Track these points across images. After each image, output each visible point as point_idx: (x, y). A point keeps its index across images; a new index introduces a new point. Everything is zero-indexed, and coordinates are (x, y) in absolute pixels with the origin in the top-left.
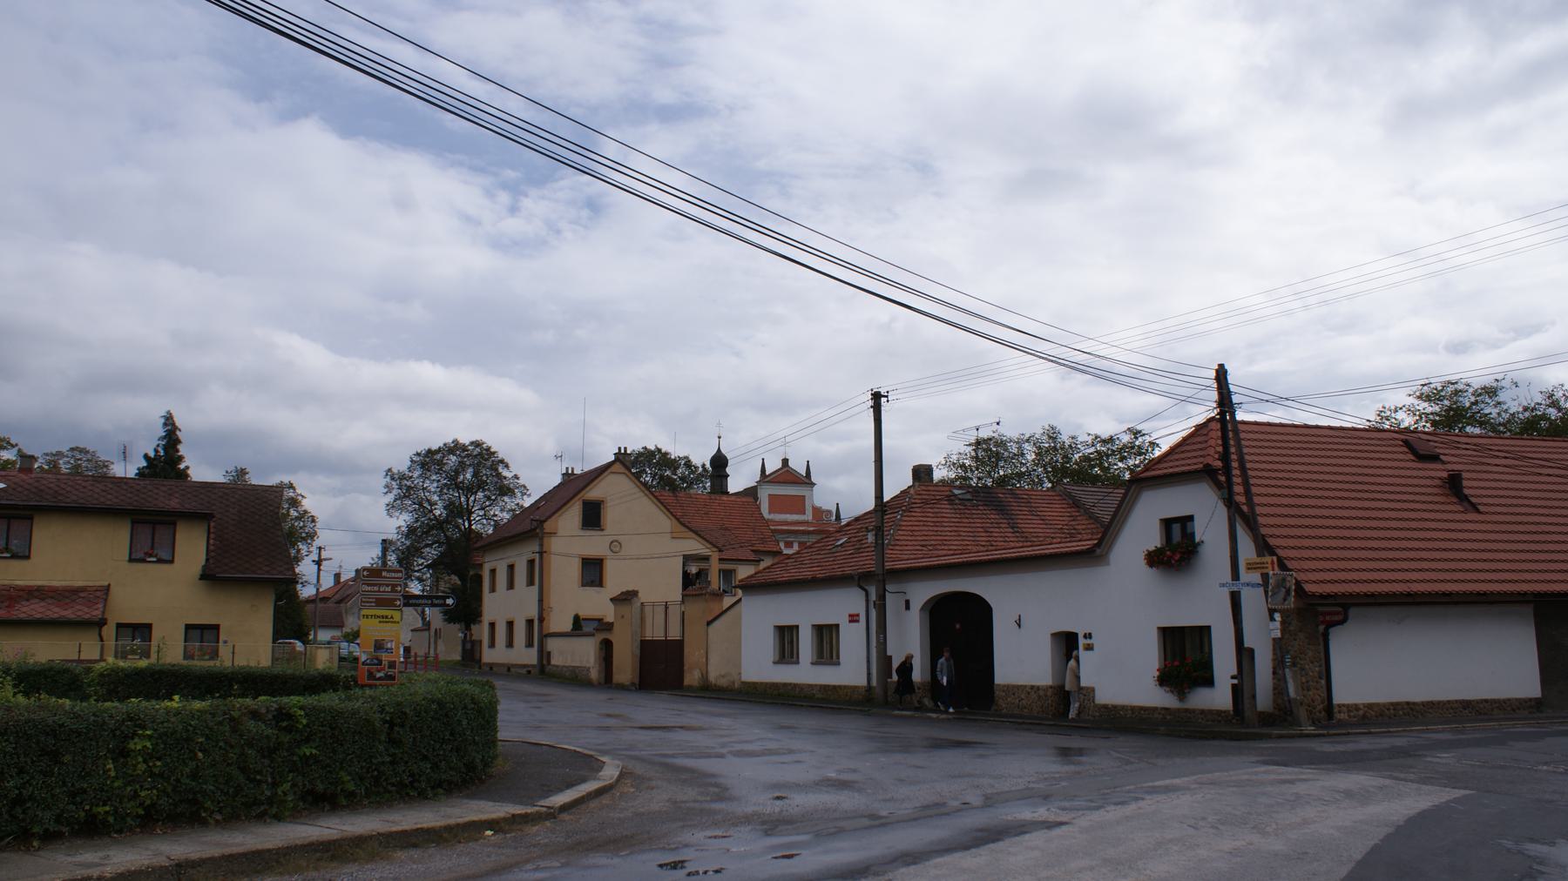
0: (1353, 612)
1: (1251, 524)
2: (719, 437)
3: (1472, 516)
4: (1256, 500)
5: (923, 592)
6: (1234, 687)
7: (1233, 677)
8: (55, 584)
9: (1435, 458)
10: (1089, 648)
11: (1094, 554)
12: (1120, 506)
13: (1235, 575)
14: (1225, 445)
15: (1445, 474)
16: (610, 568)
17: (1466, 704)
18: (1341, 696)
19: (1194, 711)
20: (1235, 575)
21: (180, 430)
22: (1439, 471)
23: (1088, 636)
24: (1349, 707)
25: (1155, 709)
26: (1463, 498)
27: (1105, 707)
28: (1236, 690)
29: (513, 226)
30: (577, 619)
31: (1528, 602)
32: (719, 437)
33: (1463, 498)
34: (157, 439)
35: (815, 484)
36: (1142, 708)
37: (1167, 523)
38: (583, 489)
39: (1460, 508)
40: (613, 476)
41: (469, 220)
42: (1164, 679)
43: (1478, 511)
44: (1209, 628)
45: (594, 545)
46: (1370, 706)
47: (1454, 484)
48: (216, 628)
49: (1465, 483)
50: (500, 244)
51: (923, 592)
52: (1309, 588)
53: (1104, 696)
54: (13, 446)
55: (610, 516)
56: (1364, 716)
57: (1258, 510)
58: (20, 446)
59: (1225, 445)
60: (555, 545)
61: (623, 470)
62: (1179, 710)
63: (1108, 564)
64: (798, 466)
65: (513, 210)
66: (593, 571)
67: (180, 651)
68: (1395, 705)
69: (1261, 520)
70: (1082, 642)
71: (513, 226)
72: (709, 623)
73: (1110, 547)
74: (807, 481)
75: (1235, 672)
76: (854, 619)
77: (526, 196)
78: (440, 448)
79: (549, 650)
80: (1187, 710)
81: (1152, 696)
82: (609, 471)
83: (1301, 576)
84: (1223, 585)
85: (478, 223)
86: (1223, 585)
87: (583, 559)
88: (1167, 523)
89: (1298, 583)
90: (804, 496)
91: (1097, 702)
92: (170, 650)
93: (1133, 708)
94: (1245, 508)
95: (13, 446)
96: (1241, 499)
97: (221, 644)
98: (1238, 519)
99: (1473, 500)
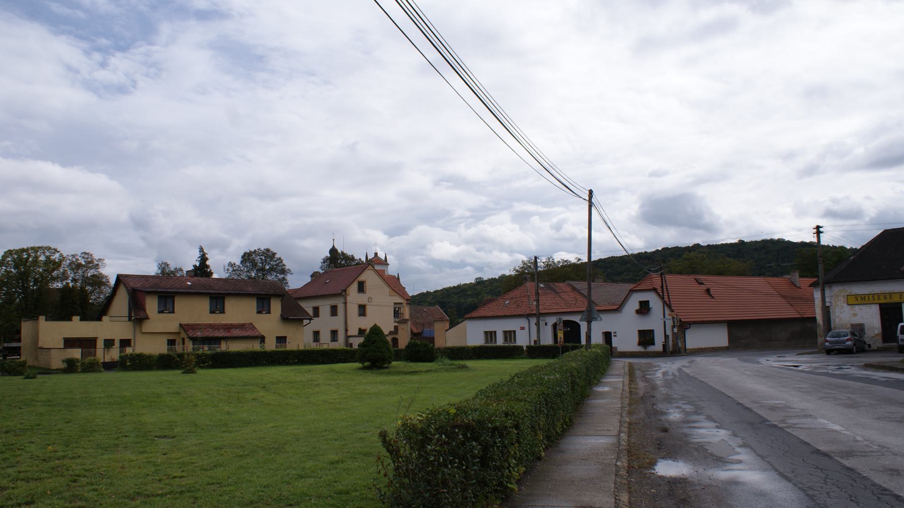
0: (691, 325)
1: (669, 307)
2: (334, 240)
3: (713, 300)
4: (671, 300)
5: (552, 320)
6: (663, 345)
7: (663, 342)
8: (234, 322)
9: (702, 284)
10: (615, 336)
11: (618, 309)
12: (626, 296)
13: (664, 317)
14: (662, 284)
15: (705, 288)
16: (369, 310)
17: (713, 348)
18: (687, 347)
19: (649, 352)
20: (664, 317)
21: (207, 254)
22: (703, 287)
23: (615, 333)
24: (690, 349)
25: (636, 352)
26: (710, 295)
27: (621, 352)
28: (664, 346)
29: (103, 75)
30: (360, 330)
31: (725, 322)
32: (334, 240)
33: (710, 295)
34: (198, 257)
35: (333, 251)
36: (632, 352)
37: (641, 303)
38: (358, 276)
39: (709, 298)
40: (368, 271)
41: (69, 68)
42: (639, 344)
43: (714, 298)
44: (653, 330)
45: (362, 299)
46: (694, 349)
47: (708, 291)
48: (285, 338)
49: (711, 291)
50: (91, 86)
51: (552, 320)
52: (682, 320)
53: (620, 349)
54: (59, 252)
55: (368, 286)
56: (692, 351)
57: (672, 303)
58: (61, 252)
59: (662, 284)
60: (349, 299)
61: (372, 268)
62: (644, 352)
63: (622, 312)
64: (382, 256)
65: (103, 65)
66: (362, 311)
67: (275, 346)
68: (699, 349)
69: (672, 305)
70: (613, 334)
71: (103, 75)
72: (446, 331)
73: (623, 307)
74: (386, 263)
75: (664, 341)
76: (522, 328)
77: (114, 56)
78: (255, 250)
79: (351, 342)
80: (647, 352)
81: (640, 349)
82: (367, 269)
83: (681, 317)
84: (662, 319)
85: (77, 72)
86: (662, 319)
87: (359, 305)
88: (641, 303)
89: (680, 319)
90: (384, 270)
91: (618, 351)
92: (271, 345)
93: (630, 352)
94: (668, 303)
95: (59, 252)
96: (666, 300)
97: (287, 343)
98: (665, 305)
99: (713, 295)
